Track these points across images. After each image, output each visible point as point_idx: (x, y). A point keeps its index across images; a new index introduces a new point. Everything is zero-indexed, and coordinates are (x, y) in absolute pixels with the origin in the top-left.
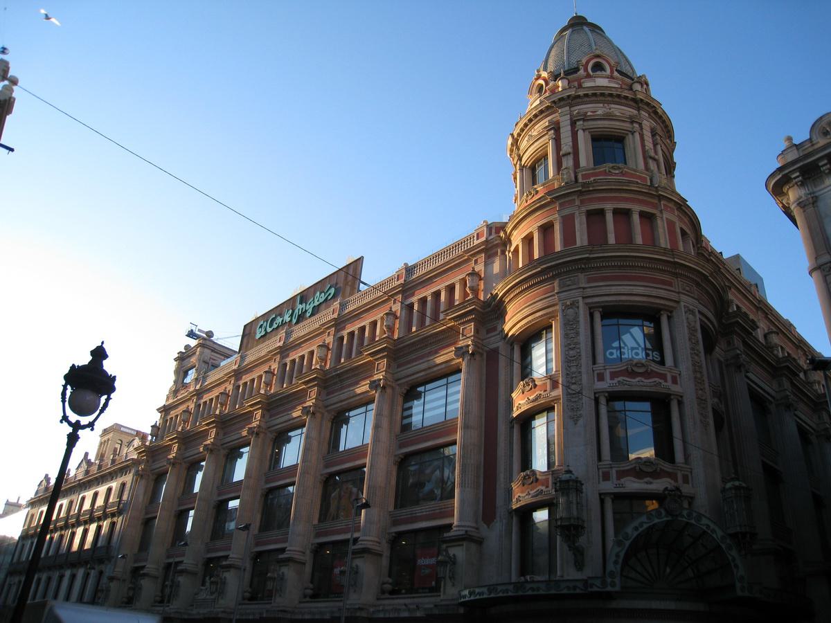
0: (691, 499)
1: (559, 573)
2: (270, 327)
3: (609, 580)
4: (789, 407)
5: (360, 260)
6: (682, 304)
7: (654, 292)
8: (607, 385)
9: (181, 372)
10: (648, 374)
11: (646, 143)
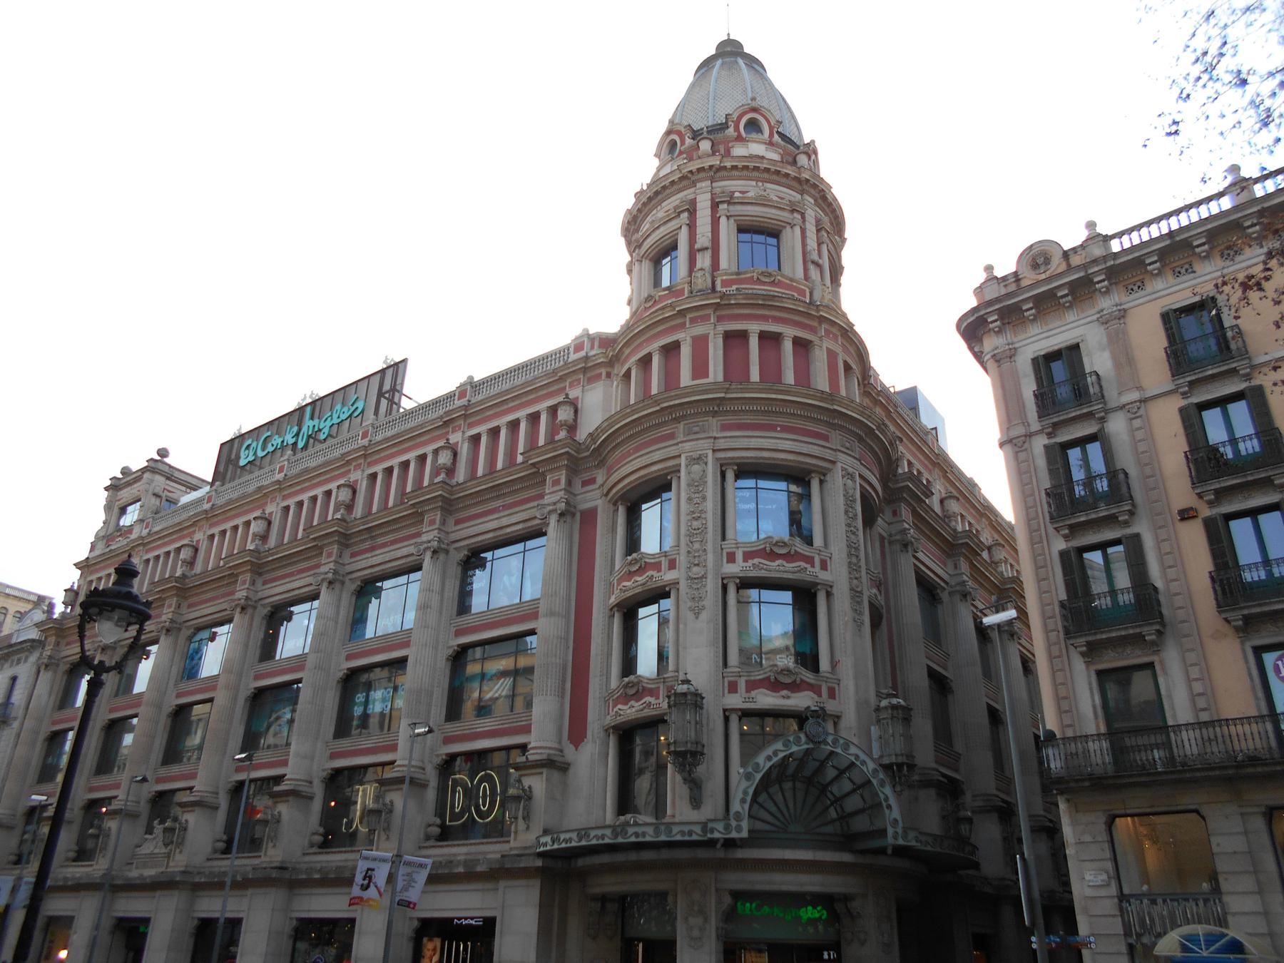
0: (837, 719)
1: (669, 812)
2: (263, 450)
3: (734, 823)
4: (965, 596)
5: (404, 361)
6: (839, 465)
7: (805, 449)
8: (736, 569)
9: (116, 508)
10: (789, 557)
11: (809, 241)
